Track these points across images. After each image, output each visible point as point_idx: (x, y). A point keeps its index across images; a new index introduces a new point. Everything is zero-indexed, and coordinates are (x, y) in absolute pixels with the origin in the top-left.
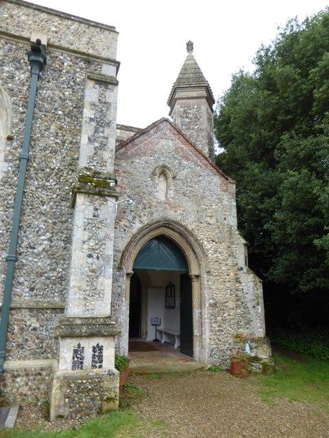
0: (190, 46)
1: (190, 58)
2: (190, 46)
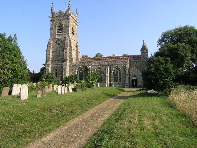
0: (144, 41)
1: (144, 44)
2: (144, 41)
